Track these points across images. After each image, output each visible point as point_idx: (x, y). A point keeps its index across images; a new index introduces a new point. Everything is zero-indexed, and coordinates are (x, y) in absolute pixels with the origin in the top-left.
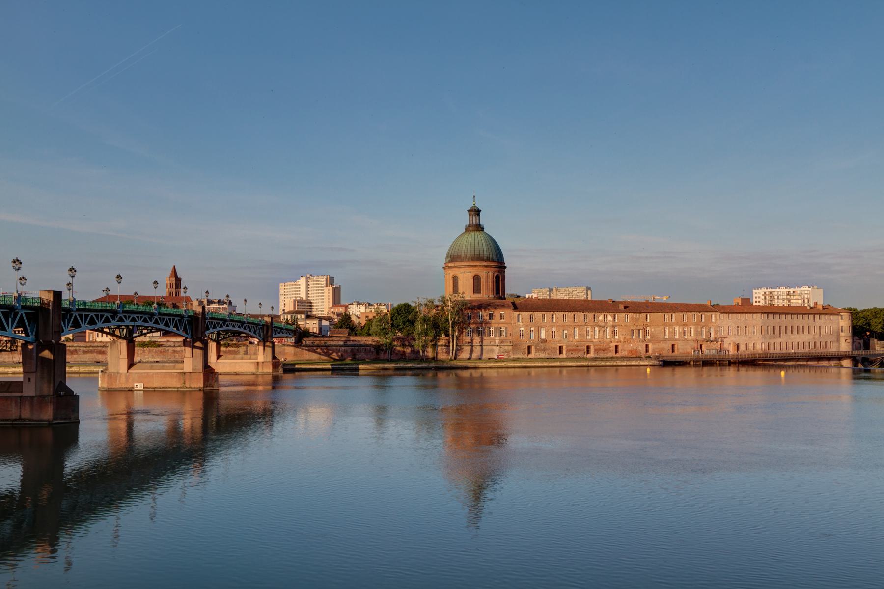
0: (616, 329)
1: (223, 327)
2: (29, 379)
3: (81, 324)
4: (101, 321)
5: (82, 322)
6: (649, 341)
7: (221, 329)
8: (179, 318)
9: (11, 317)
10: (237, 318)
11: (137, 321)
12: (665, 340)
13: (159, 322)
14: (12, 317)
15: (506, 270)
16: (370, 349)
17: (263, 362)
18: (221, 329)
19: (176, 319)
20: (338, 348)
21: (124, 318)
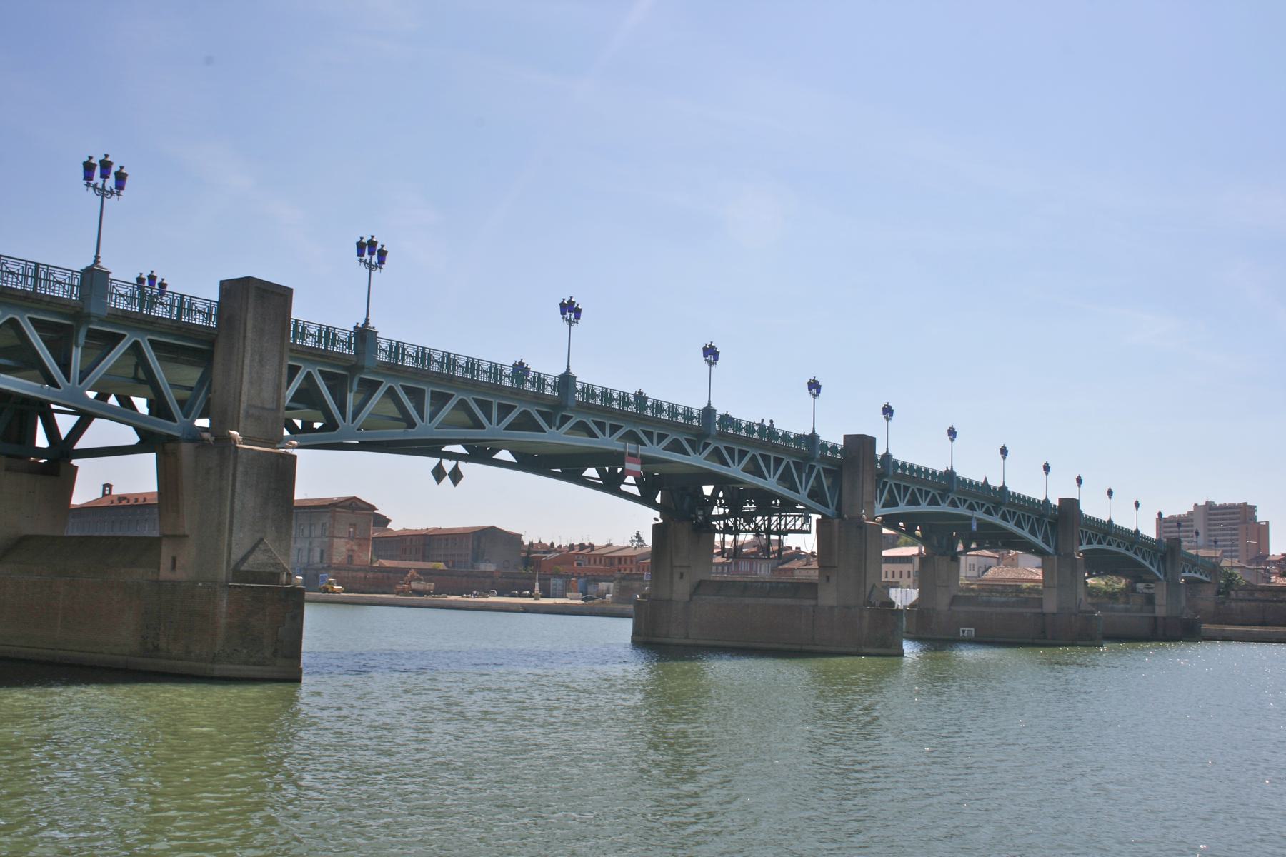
1: (1102, 544)
2: (828, 578)
3: (920, 500)
5: (922, 498)
8: (1037, 517)
11: (976, 511)
13: (1008, 517)
14: (807, 471)
21: (975, 506)
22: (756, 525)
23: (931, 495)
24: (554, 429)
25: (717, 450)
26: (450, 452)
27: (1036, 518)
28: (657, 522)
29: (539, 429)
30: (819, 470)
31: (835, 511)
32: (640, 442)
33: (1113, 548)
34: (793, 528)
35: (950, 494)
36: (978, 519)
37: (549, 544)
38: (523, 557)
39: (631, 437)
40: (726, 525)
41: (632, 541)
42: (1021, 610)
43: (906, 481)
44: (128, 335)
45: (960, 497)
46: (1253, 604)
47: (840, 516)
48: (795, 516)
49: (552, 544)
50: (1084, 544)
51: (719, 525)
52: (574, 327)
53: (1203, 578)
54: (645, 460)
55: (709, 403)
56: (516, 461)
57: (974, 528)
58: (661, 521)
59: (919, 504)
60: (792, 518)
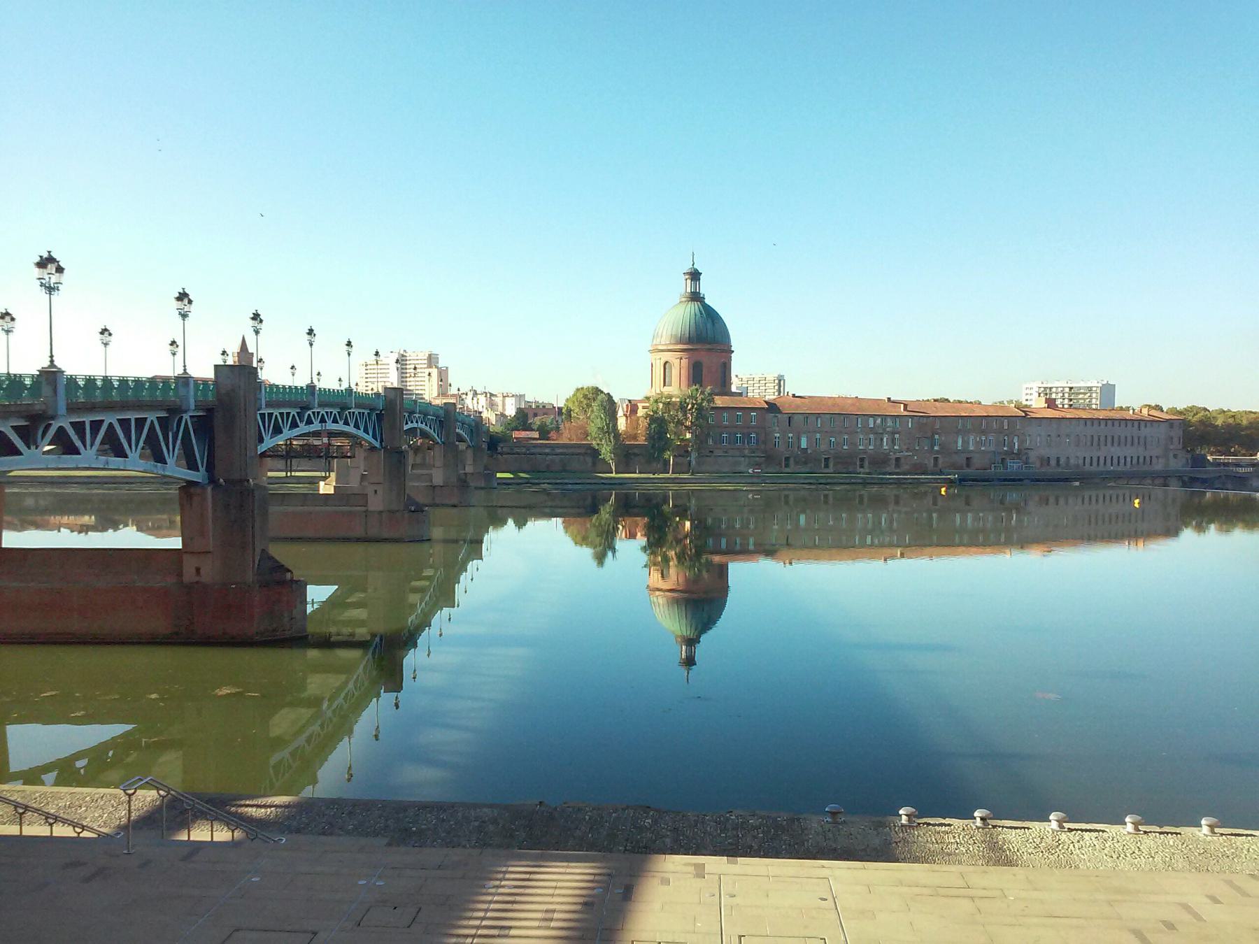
0: (897, 436)
2: (376, 491)
6: (938, 452)
7: (296, 432)
9: (172, 429)
10: (1117, 415)
12: (957, 452)
15: (733, 355)
17: (472, 474)
18: (296, 432)
19: (152, 417)
27: (338, 412)
31: (205, 473)
38: (706, 519)
47: (212, 480)
50: (266, 438)
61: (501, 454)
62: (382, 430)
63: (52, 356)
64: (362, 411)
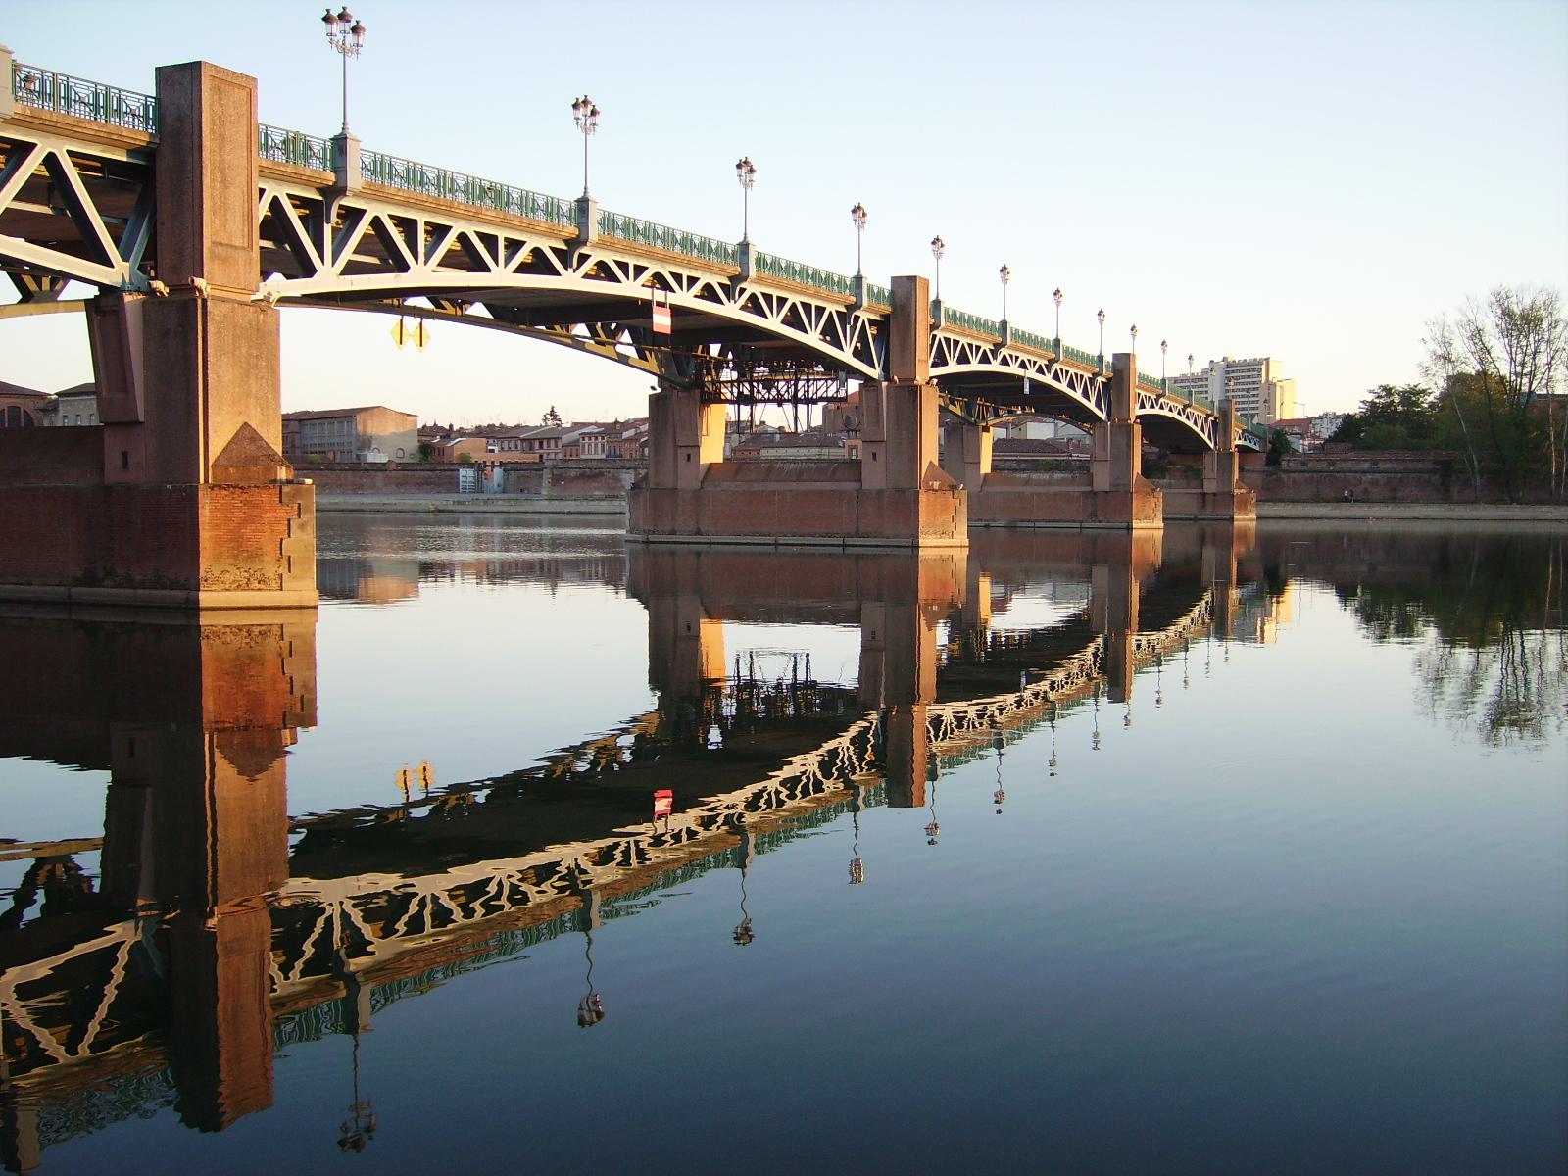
2: (874, 455)
3: (948, 357)
4: (778, 314)
9: (849, 324)
16: (1429, 478)
17: (1215, 494)
20: (1358, 476)
22: (779, 391)
23: (787, 306)
24: (571, 270)
25: (753, 297)
26: (414, 307)
28: (655, 392)
29: (553, 272)
30: (864, 322)
32: (666, 287)
33: (1165, 412)
34: (825, 395)
35: (743, 285)
36: (1031, 380)
37: (447, 427)
39: (659, 281)
40: (740, 393)
41: (545, 420)
42: (1069, 489)
43: (639, 255)
44: (40, 145)
45: (678, 270)
46: (1307, 475)
48: (826, 380)
49: (451, 426)
51: (726, 393)
52: (351, 60)
53: (1252, 445)
54: (677, 311)
55: (859, 272)
56: (492, 317)
57: (1027, 390)
58: (659, 390)
59: (970, 362)
60: (823, 382)
61: (1287, 472)
62: (1110, 396)
63: (745, 234)
64: (1200, 414)
